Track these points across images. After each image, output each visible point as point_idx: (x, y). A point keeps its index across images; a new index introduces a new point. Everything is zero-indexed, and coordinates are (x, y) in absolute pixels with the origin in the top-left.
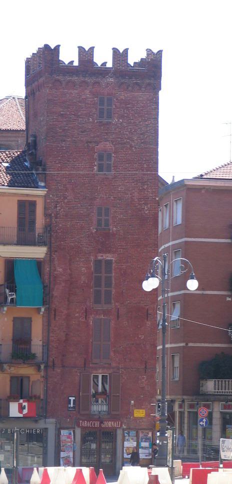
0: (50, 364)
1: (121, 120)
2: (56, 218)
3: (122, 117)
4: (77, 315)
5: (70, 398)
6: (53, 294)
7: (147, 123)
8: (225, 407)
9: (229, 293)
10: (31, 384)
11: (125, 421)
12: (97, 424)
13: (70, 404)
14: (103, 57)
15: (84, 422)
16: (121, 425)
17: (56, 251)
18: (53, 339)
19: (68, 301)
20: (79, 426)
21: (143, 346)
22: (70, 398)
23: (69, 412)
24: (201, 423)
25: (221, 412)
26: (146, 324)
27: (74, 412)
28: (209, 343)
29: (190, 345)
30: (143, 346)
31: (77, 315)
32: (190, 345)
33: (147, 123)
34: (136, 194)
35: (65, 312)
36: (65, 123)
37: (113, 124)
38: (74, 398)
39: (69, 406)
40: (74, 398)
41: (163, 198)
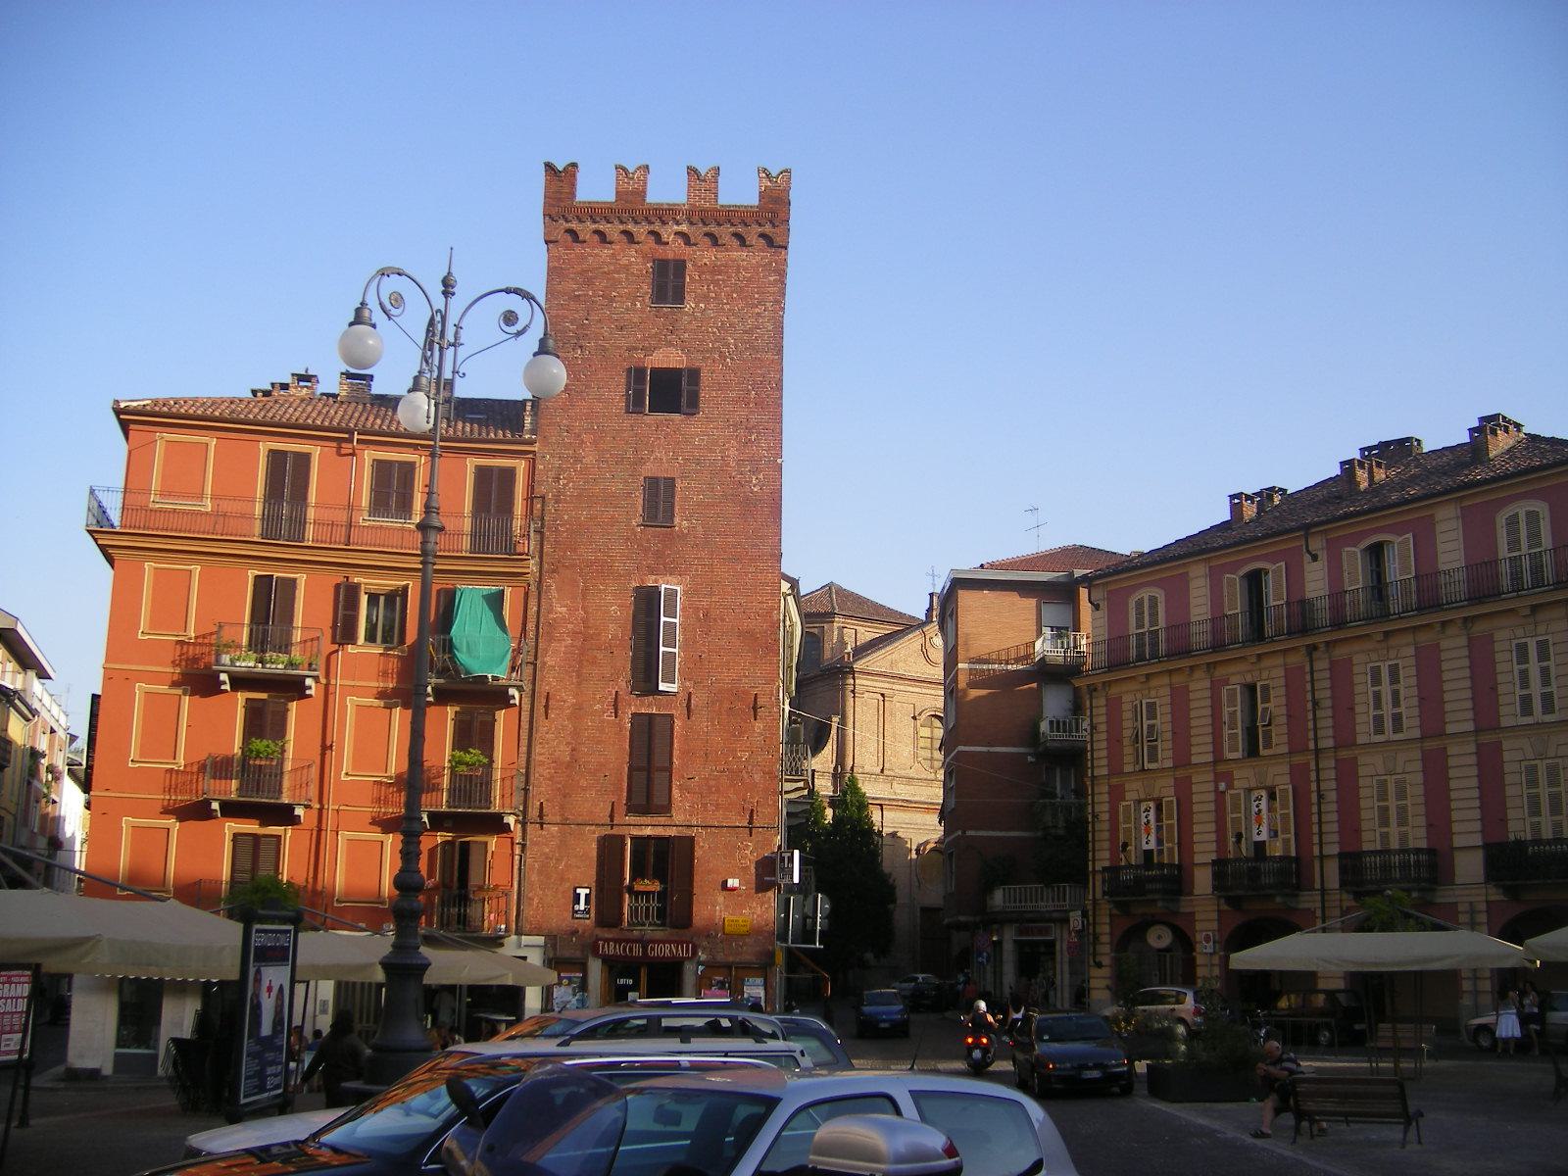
0: (533, 813)
1: (702, 305)
2: (556, 503)
3: (705, 298)
4: (597, 707)
5: (578, 891)
6: (545, 663)
7: (757, 310)
8: (1021, 932)
9: (1031, 751)
10: (489, 858)
11: (705, 943)
12: (637, 950)
13: (579, 904)
14: (667, 189)
15: (608, 944)
16: (695, 953)
17: (554, 571)
18: (541, 758)
19: (578, 676)
20: (596, 954)
21: (746, 776)
22: (578, 891)
23: (576, 921)
24: (980, 959)
25: (1015, 941)
26: (753, 727)
27: (587, 921)
28: (1001, 831)
29: (970, 833)
30: (746, 776)
31: (597, 707)
32: (970, 833)
33: (757, 310)
34: (733, 452)
35: (571, 700)
36: (581, 313)
37: (687, 314)
38: (587, 891)
39: (577, 907)
40: (587, 891)
41: (1072, 758)
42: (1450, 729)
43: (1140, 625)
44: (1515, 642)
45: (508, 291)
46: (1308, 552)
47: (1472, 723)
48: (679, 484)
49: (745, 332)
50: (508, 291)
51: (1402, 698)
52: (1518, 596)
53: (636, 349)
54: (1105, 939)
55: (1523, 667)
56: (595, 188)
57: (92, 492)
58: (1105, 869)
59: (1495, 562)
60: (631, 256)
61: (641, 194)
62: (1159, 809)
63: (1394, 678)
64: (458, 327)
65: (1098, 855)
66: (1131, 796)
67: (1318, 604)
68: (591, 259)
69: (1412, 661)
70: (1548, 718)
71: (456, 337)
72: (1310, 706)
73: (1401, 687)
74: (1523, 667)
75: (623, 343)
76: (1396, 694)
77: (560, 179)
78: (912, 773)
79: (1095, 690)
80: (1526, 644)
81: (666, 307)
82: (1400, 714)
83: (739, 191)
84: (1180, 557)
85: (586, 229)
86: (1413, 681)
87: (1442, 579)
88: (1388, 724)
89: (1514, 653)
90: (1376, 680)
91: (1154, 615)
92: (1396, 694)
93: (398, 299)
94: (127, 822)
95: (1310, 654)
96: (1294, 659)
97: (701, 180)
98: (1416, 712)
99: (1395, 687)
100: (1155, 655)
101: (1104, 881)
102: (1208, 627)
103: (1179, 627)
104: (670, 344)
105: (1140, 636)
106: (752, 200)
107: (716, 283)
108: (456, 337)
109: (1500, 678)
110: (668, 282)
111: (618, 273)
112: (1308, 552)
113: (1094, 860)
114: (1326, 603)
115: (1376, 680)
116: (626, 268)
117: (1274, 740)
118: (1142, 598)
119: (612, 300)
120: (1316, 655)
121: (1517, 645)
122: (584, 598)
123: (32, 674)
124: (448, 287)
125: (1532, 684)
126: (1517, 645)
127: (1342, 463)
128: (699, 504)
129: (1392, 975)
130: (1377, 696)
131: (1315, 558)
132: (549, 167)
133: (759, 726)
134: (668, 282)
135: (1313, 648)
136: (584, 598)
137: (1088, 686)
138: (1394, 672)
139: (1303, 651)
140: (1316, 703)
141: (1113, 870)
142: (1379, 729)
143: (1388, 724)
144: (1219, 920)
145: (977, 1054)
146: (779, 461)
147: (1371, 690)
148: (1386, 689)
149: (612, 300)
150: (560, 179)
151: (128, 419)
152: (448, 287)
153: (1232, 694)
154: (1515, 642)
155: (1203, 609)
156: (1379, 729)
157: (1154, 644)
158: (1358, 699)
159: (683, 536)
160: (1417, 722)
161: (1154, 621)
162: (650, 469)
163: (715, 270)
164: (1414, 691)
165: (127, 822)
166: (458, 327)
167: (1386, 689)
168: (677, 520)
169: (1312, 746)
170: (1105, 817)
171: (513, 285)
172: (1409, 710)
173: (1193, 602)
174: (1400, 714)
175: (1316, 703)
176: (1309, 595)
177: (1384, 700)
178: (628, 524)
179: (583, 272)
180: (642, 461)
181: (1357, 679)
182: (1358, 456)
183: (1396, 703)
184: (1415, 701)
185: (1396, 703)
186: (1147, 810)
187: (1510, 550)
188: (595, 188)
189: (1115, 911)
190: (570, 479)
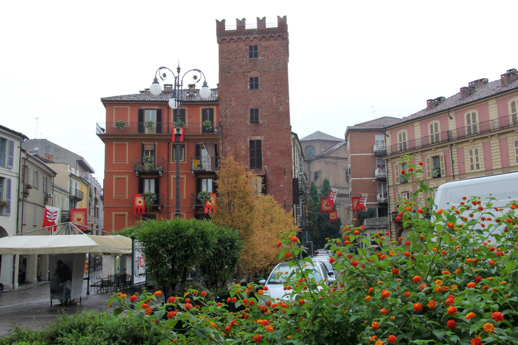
3: (264, 56)
14: (251, 25)
34: (274, 100)
37: (259, 61)
42: (494, 168)
43: (400, 141)
44: (514, 140)
45: (194, 70)
46: (449, 116)
47: (484, 168)
48: (260, 110)
49: (276, 65)
50: (194, 70)
51: (479, 159)
52: (515, 126)
53: (245, 72)
54: (394, 233)
55: (471, 156)
56: (231, 26)
57: (97, 124)
58: (393, 213)
59: (508, 116)
60: (242, 45)
61: (244, 27)
62: (408, 194)
63: (476, 153)
64: (182, 81)
65: (391, 209)
66: (400, 191)
67: (453, 132)
68: (230, 47)
69: (482, 148)
70: (478, 170)
71: (182, 83)
72: (451, 162)
73: (479, 155)
74: (471, 156)
75: (241, 71)
76: (477, 158)
77: (221, 25)
78: (344, 186)
79: (388, 160)
80: (472, 150)
81: (253, 59)
82: (479, 164)
83: (272, 23)
84: (411, 120)
85: (228, 38)
86: (482, 154)
87: (491, 122)
88: (475, 167)
89: (514, 144)
90: (471, 153)
91: (404, 138)
92: (477, 158)
93: (164, 75)
94: (114, 213)
95: (451, 147)
96: (446, 149)
97: (261, 22)
98: (483, 163)
99: (477, 156)
100: (405, 149)
101: (392, 216)
102: (420, 140)
103: (412, 141)
104: (254, 70)
105: (401, 144)
106: (276, 25)
107: (267, 51)
108: (182, 83)
109: (510, 152)
110: (253, 52)
111: (238, 50)
112: (449, 116)
113: (390, 210)
114: (455, 131)
115: (471, 153)
116: (241, 49)
117: (480, 166)
118: (514, 101)
119: (237, 58)
120: (453, 147)
121: (470, 150)
122: (235, 144)
123: (88, 173)
124: (179, 69)
125: (474, 161)
126: (470, 150)
127: (461, 89)
128: (265, 115)
129: (73, 255)
130: (471, 159)
131: (451, 118)
132: (217, 21)
133: (286, 177)
134: (253, 52)
135: (452, 145)
136: (235, 144)
137: (386, 159)
138: (476, 151)
139: (449, 146)
140: (453, 162)
141: (396, 213)
142: (472, 168)
143: (475, 167)
144: (395, 228)
145: (220, 263)
146: (288, 101)
147: (469, 157)
148: (474, 156)
149: (237, 58)
150: (221, 25)
151: (107, 102)
152: (179, 69)
153: (428, 160)
154: (514, 140)
155: (419, 135)
156: (472, 168)
157: (405, 146)
158: (466, 160)
159: (261, 125)
160: (484, 166)
161: (474, 121)
162: (251, 106)
163: (266, 47)
164: (483, 157)
165: (114, 213)
166: (182, 81)
167: (474, 156)
168: (259, 120)
169: (452, 174)
170: (392, 197)
171: (195, 69)
172: (481, 162)
173: (416, 133)
174: (479, 164)
175: (453, 162)
176: (450, 129)
177: (473, 160)
178: (246, 122)
179: (228, 51)
180: (249, 104)
181: (465, 154)
182: (467, 86)
183: (477, 160)
184: (483, 160)
185: (477, 160)
186: (405, 195)
187: (468, 124)
188: (231, 26)
189: (396, 225)
190: (228, 111)
